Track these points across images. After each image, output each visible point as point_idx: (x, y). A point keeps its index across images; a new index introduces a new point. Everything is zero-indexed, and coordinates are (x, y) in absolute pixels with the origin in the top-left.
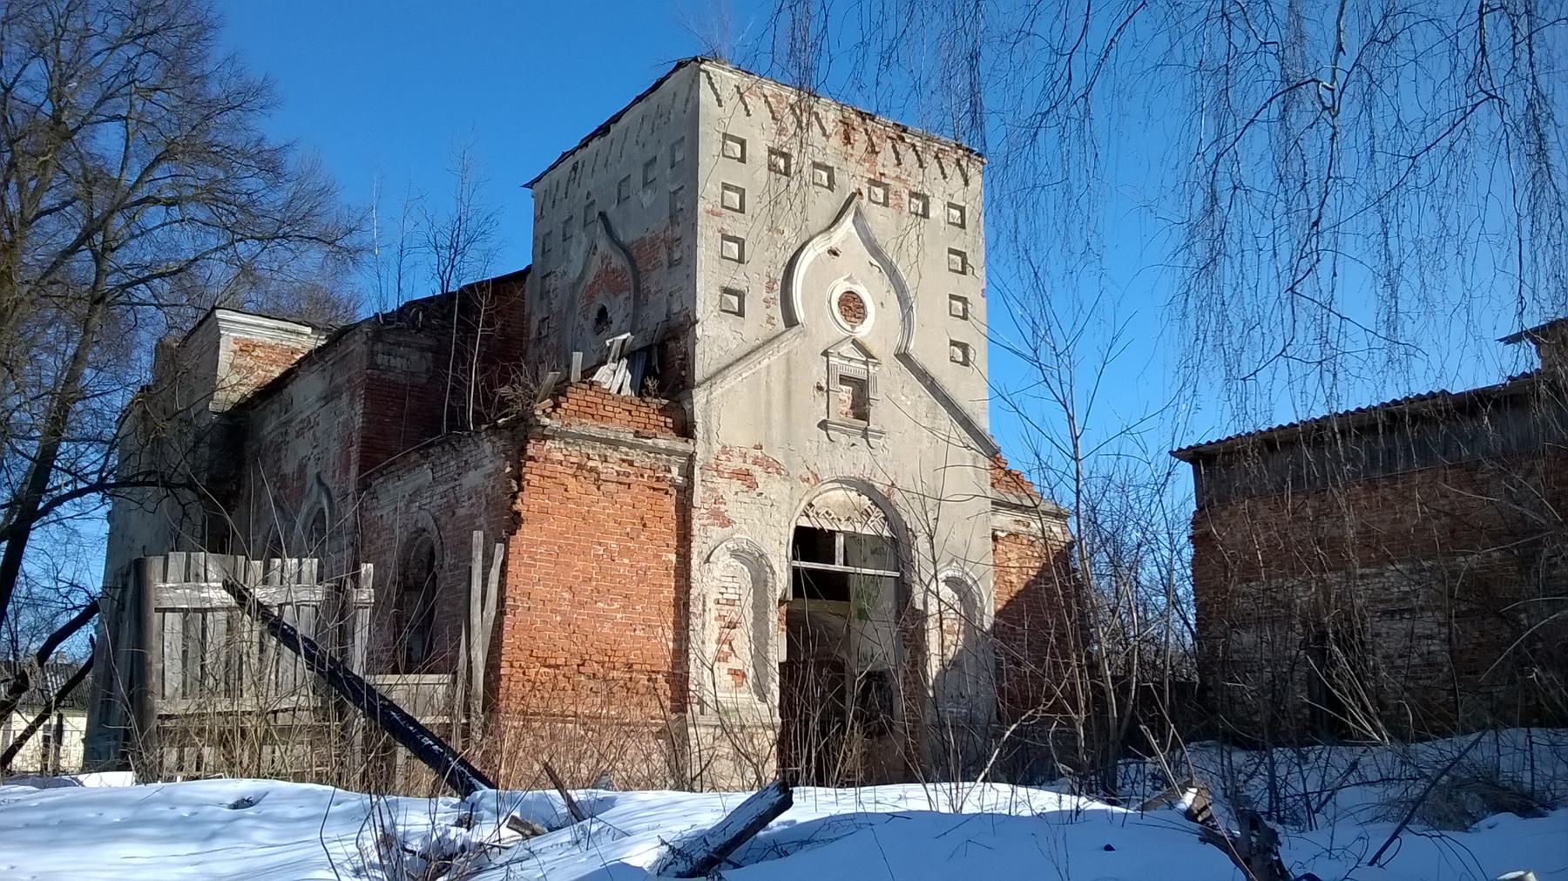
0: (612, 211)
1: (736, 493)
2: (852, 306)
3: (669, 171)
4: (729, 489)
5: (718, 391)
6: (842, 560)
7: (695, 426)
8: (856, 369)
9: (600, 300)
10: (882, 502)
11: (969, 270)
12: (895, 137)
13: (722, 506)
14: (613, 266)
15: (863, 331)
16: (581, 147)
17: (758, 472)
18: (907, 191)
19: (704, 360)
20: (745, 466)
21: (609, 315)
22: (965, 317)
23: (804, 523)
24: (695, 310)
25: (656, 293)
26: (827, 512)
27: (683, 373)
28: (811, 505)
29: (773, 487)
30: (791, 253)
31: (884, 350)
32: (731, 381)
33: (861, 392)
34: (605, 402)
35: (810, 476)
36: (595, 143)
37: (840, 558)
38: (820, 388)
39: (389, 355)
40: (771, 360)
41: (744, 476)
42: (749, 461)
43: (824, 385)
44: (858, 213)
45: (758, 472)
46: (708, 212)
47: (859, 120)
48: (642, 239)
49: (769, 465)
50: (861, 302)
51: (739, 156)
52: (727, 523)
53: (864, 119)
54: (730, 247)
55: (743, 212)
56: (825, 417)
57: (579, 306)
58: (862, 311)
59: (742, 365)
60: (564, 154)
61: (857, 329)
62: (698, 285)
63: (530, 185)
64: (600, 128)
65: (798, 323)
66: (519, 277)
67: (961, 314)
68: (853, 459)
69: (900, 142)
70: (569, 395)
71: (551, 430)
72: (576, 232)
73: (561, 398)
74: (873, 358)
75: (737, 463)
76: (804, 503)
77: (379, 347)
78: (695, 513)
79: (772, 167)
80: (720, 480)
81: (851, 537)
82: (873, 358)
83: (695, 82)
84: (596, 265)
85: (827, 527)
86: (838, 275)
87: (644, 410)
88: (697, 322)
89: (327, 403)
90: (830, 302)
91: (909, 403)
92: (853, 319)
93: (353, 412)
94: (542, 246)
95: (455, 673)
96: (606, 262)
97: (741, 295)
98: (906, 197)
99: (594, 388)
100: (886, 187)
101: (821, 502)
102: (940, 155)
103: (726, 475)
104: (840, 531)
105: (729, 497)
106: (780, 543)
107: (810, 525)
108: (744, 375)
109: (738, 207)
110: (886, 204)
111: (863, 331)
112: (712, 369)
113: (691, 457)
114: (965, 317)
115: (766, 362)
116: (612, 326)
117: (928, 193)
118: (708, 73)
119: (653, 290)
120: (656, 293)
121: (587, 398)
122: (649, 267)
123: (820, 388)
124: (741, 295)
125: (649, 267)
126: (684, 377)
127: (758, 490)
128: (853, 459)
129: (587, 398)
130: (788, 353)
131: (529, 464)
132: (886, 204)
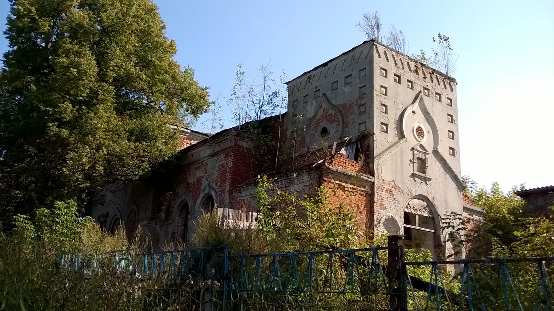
0: (328, 94)
1: (387, 198)
2: (420, 132)
3: (358, 80)
4: (385, 195)
5: (381, 160)
6: (418, 225)
7: (374, 172)
8: (421, 156)
9: (324, 124)
10: (431, 206)
11: (454, 122)
12: (431, 72)
13: (383, 202)
14: (329, 113)
15: (424, 141)
16: (313, 70)
17: (393, 190)
18: (435, 92)
19: (377, 148)
20: (390, 188)
21: (328, 131)
22: (453, 139)
23: (406, 210)
24: (373, 130)
25: (352, 123)
26: (413, 207)
27: (368, 153)
28: (409, 204)
29: (398, 196)
30: (399, 113)
31: (430, 149)
32: (384, 157)
33: (422, 164)
34: (346, 162)
35: (409, 193)
36: (320, 69)
37: (417, 224)
38: (411, 161)
39: (241, 141)
40: (396, 150)
41: (389, 191)
42: (391, 186)
43: (412, 160)
44: (421, 98)
45: (393, 190)
46: (377, 95)
47: (421, 65)
48: (345, 104)
49: (397, 188)
50: (423, 131)
51: (385, 75)
52: (385, 209)
53: (422, 66)
54: (383, 108)
55: (387, 96)
56: (413, 172)
57: (312, 127)
58: (423, 134)
59: (389, 151)
60: (305, 73)
61: (422, 141)
62: (374, 121)
63: (287, 83)
64: (324, 64)
65: (405, 137)
66: (283, 115)
67: (452, 137)
68: (420, 188)
69: (432, 74)
70: (335, 158)
71: (331, 170)
72: (310, 100)
73: (333, 159)
74: (427, 151)
75: (387, 187)
76: (407, 203)
77: (238, 138)
78: (375, 204)
79: (395, 80)
80: (382, 193)
81: (421, 217)
82: (427, 151)
83: (371, 48)
84: (321, 112)
85: (414, 212)
86: (415, 121)
87: (357, 165)
88: (374, 134)
89: (212, 157)
90: (413, 130)
91: (438, 169)
92: (420, 137)
93: (227, 161)
94: (292, 103)
95: (3, 257)
96: (325, 112)
97: (386, 125)
98: (434, 94)
99: (343, 156)
100: (428, 90)
101: (412, 203)
102: (445, 80)
103: (384, 191)
104: (417, 214)
105: (385, 199)
106: (401, 217)
107: (408, 211)
108: (389, 155)
109: (385, 94)
110: (428, 96)
111: (424, 141)
112: (379, 152)
113: (373, 183)
114: (453, 139)
115: (395, 151)
116: (330, 135)
117: (441, 94)
118: (376, 45)
119: (351, 122)
120: (352, 123)
121: (341, 160)
122: (349, 114)
123: (411, 161)
124: (386, 125)
125: (349, 114)
126: (368, 154)
127: (394, 197)
128: (420, 188)
129: (341, 160)
130: (402, 147)
131: (324, 182)
132: (428, 96)
